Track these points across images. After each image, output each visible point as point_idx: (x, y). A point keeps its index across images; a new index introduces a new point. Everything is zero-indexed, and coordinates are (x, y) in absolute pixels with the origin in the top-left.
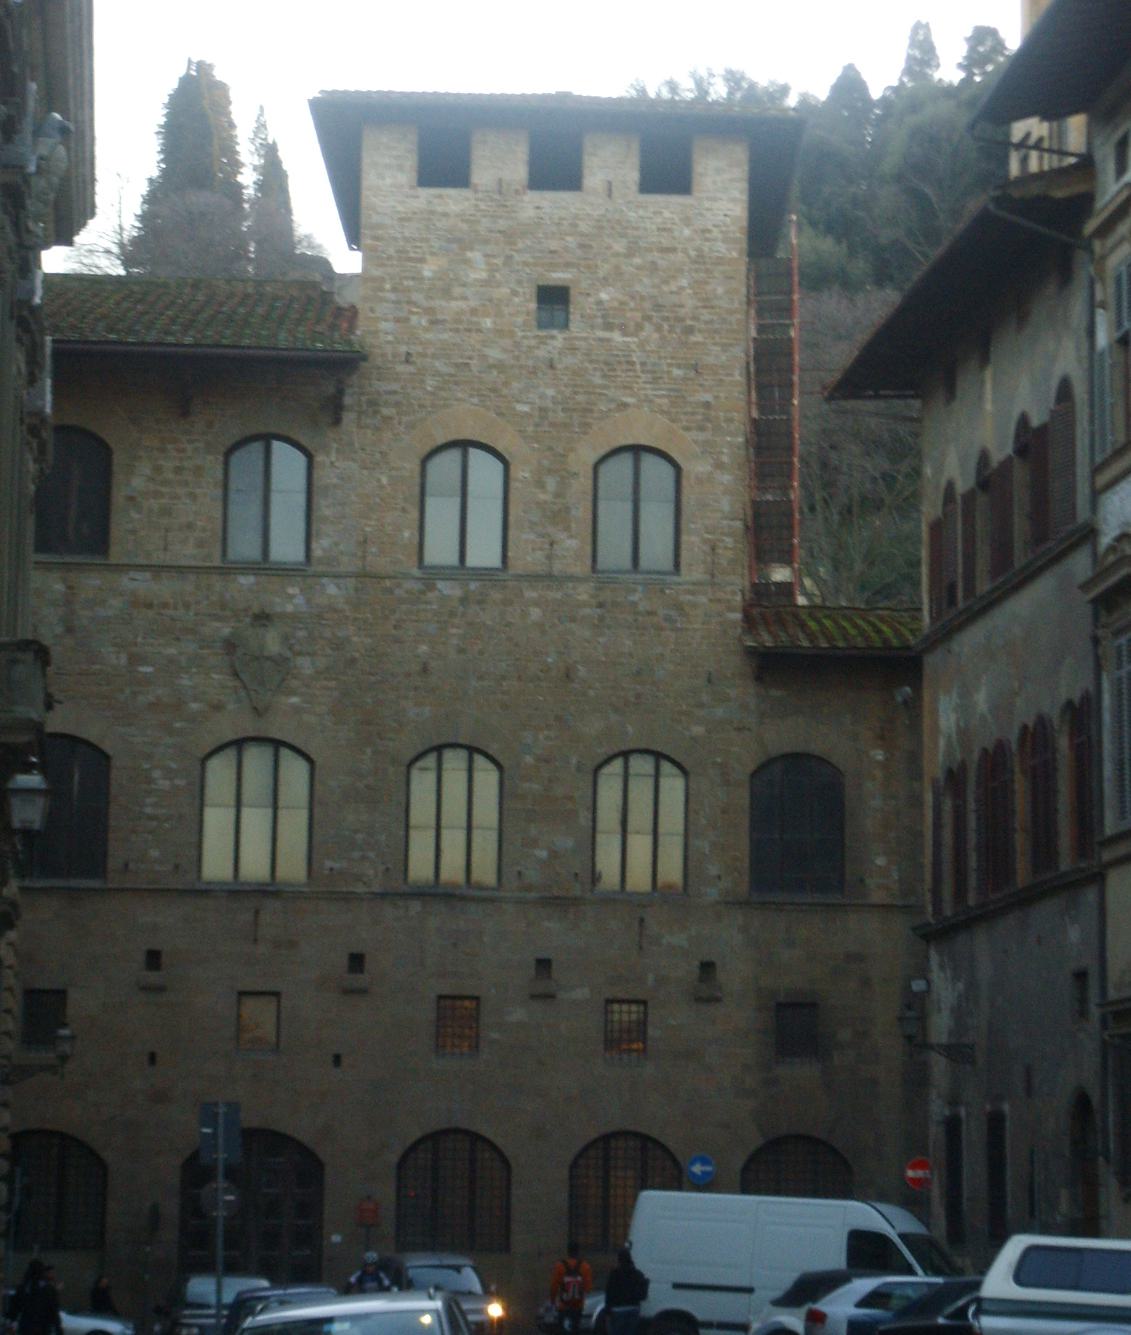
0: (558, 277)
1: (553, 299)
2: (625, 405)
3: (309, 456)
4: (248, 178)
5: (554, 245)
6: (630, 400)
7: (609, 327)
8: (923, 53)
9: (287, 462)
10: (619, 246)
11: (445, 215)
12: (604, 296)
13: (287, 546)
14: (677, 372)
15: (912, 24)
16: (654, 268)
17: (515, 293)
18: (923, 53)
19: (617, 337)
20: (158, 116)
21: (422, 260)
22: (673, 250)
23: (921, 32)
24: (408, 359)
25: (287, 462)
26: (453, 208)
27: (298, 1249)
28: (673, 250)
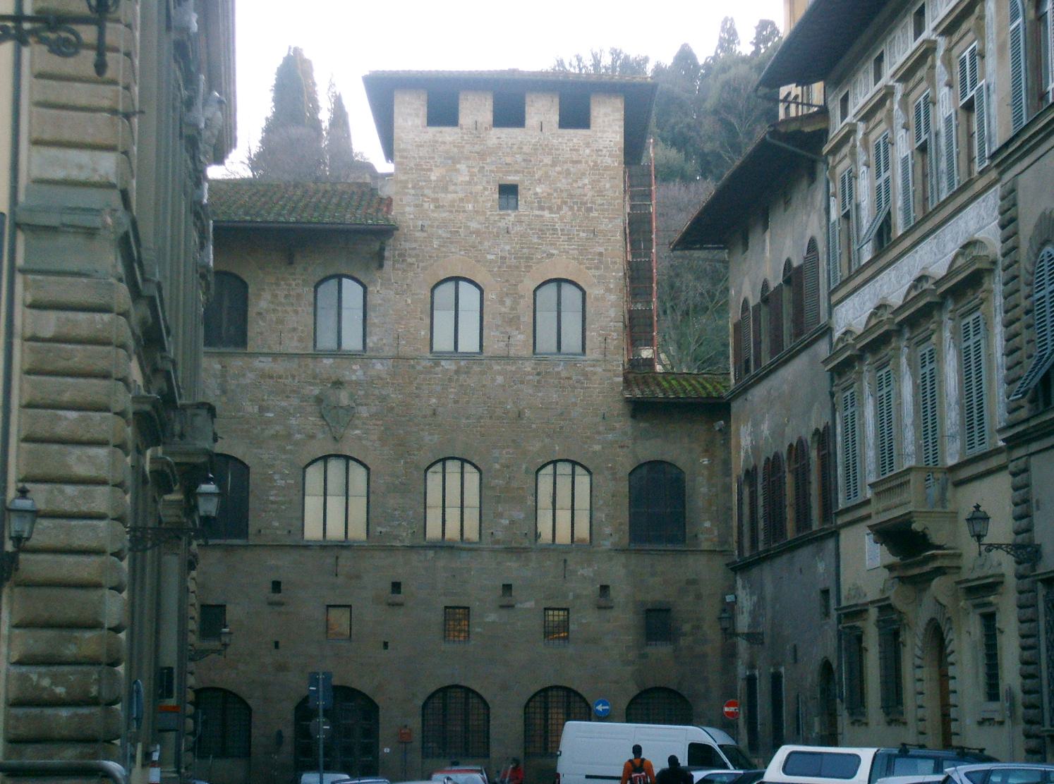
5: (508, 160)
6: (555, 252)
7: (542, 208)
8: (729, 36)
9: (351, 290)
12: (538, 190)
13: (352, 341)
16: (568, 173)
18: (729, 36)
19: (546, 214)
21: (430, 170)
25: (351, 290)
26: (448, 139)
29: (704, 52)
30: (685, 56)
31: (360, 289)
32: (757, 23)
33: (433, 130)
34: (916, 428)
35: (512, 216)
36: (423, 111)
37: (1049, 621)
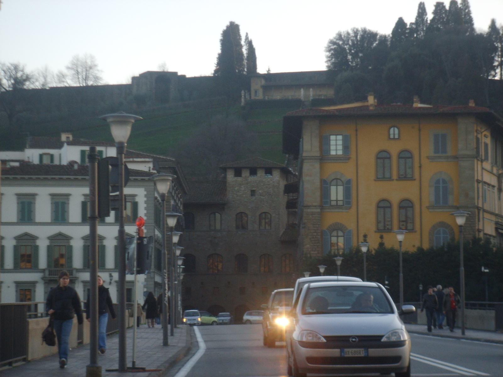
0: (254, 189)
1: (253, 193)
2: (263, 207)
3: (221, 215)
4: (245, 51)
5: (253, 185)
6: (264, 206)
7: (261, 196)
8: (422, 10)
9: (218, 215)
10: (262, 184)
11: (238, 181)
12: (260, 191)
13: (218, 227)
14: (270, 202)
15: (419, 3)
16: (267, 187)
17: (248, 191)
18: (422, 10)
19: (262, 197)
20: (219, 37)
21: (235, 187)
22: (269, 185)
23: (422, 6)
24: (233, 201)
25: (218, 215)
26: (239, 180)
27: (281, 375)
28: (269, 185)
29: (410, 19)
30: (401, 23)
31: (220, 215)
32: (435, 4)
33: (236, 178)
34: (178, 300)
35: (254, 198)
36: (233, 174)
37: (89, 290)
